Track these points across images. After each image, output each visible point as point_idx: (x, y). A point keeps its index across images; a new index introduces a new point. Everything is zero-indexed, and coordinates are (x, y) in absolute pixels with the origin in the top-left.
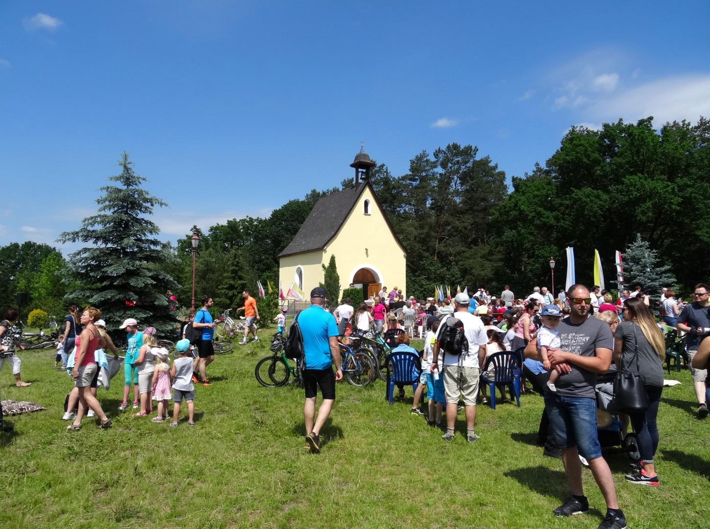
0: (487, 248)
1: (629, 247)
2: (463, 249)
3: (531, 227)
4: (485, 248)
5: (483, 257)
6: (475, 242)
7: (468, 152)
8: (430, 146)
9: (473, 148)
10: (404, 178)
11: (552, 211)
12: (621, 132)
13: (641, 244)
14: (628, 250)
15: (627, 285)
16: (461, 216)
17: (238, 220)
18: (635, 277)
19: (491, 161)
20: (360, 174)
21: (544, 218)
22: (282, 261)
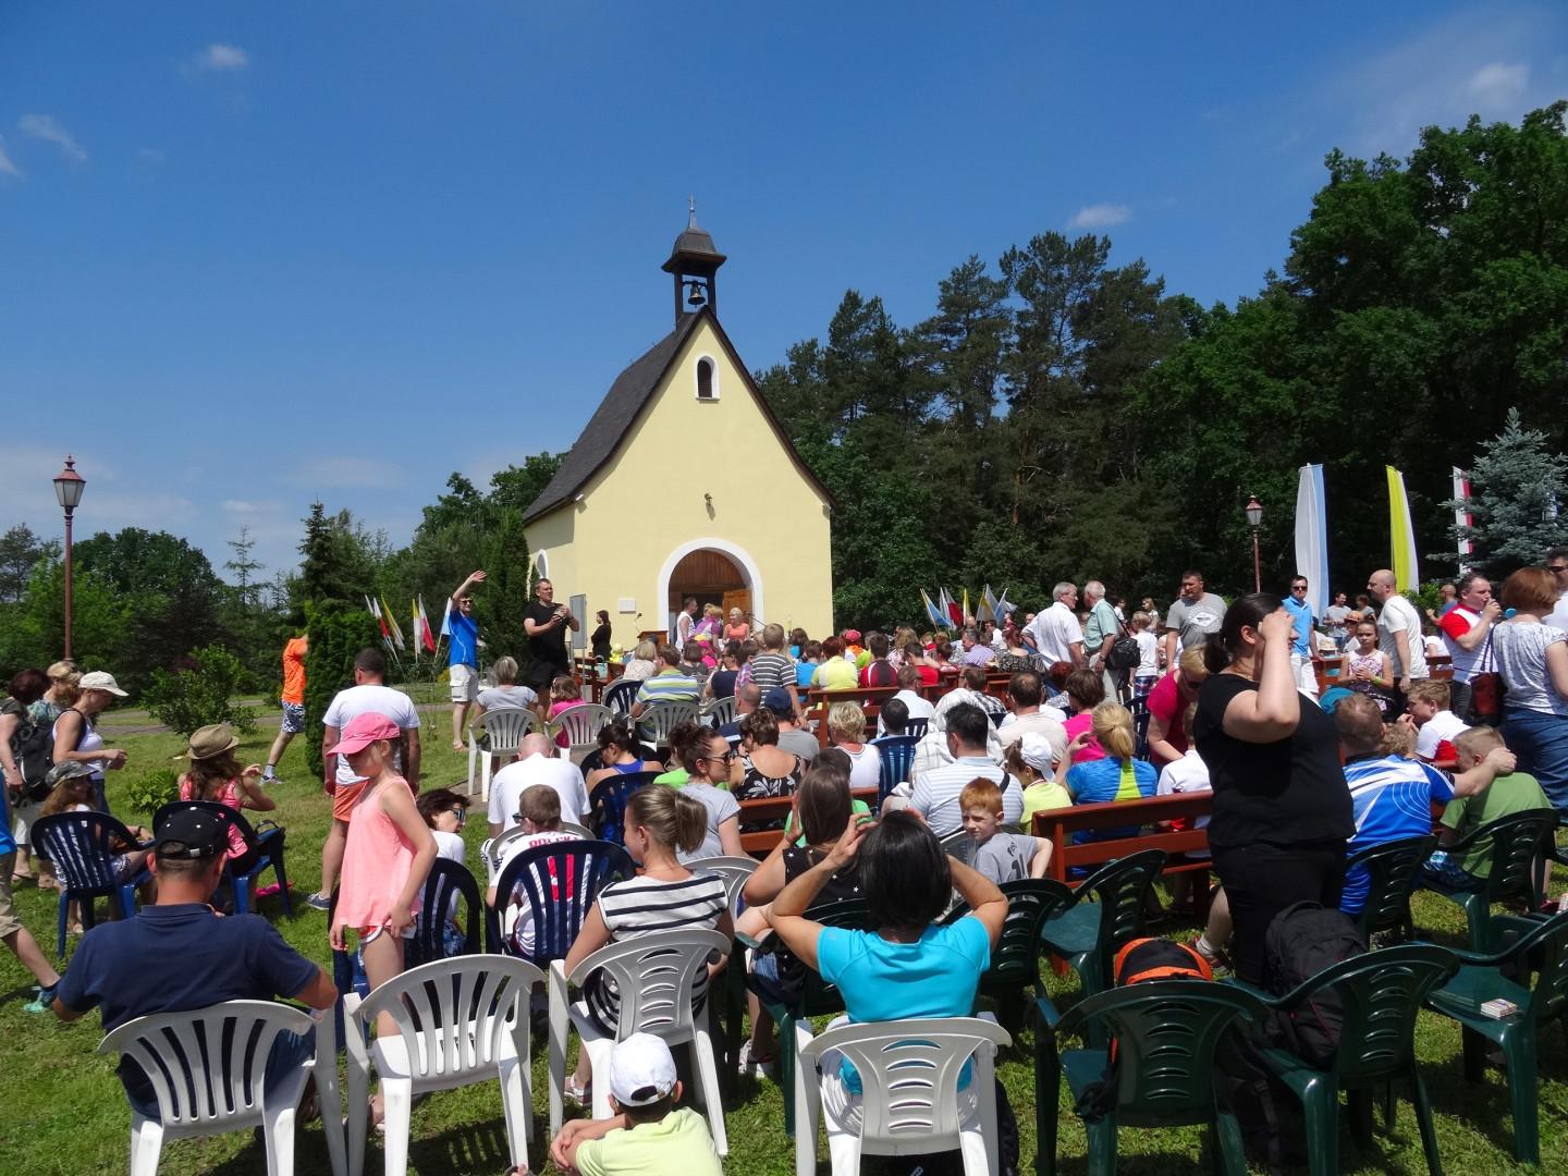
0: (1137, 489)
1: (1484, 452)
2: (1079, 494)
3: (1232, 423)
4: (1133, 489)
5: (1129, 511)
6: (1109, 477)
7: (1090, 250)
8: (990, 238)
9: (1099, 242)
10: (926, 328)
11: (1287, 379)
12: (1476, 150)
13: (1519, 438)
14: (1482, 461)
15: (1477, 564)
16: (1073, 413)
17: (552, 456)
18: (1500, 540)
19: (1147, 273)
20: (687, 289)
21: (1264, 397)
22: (530, 536)
